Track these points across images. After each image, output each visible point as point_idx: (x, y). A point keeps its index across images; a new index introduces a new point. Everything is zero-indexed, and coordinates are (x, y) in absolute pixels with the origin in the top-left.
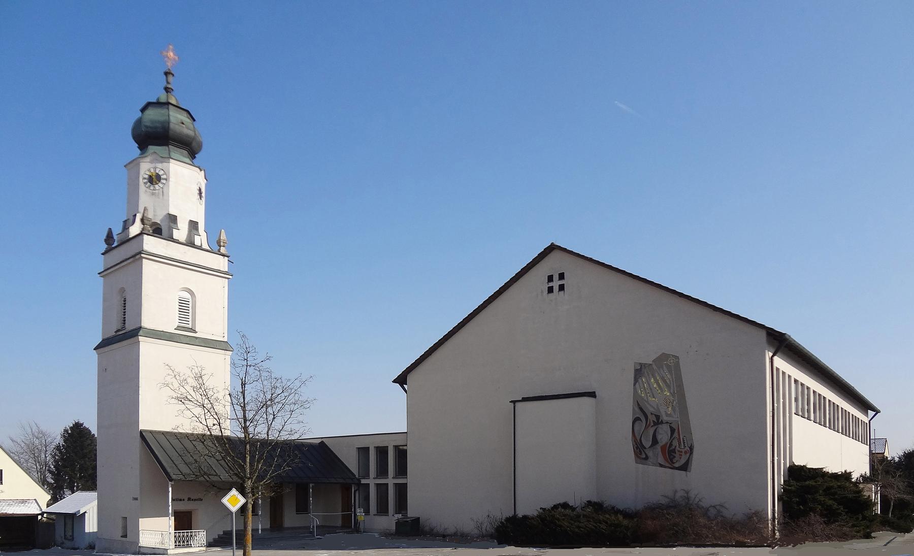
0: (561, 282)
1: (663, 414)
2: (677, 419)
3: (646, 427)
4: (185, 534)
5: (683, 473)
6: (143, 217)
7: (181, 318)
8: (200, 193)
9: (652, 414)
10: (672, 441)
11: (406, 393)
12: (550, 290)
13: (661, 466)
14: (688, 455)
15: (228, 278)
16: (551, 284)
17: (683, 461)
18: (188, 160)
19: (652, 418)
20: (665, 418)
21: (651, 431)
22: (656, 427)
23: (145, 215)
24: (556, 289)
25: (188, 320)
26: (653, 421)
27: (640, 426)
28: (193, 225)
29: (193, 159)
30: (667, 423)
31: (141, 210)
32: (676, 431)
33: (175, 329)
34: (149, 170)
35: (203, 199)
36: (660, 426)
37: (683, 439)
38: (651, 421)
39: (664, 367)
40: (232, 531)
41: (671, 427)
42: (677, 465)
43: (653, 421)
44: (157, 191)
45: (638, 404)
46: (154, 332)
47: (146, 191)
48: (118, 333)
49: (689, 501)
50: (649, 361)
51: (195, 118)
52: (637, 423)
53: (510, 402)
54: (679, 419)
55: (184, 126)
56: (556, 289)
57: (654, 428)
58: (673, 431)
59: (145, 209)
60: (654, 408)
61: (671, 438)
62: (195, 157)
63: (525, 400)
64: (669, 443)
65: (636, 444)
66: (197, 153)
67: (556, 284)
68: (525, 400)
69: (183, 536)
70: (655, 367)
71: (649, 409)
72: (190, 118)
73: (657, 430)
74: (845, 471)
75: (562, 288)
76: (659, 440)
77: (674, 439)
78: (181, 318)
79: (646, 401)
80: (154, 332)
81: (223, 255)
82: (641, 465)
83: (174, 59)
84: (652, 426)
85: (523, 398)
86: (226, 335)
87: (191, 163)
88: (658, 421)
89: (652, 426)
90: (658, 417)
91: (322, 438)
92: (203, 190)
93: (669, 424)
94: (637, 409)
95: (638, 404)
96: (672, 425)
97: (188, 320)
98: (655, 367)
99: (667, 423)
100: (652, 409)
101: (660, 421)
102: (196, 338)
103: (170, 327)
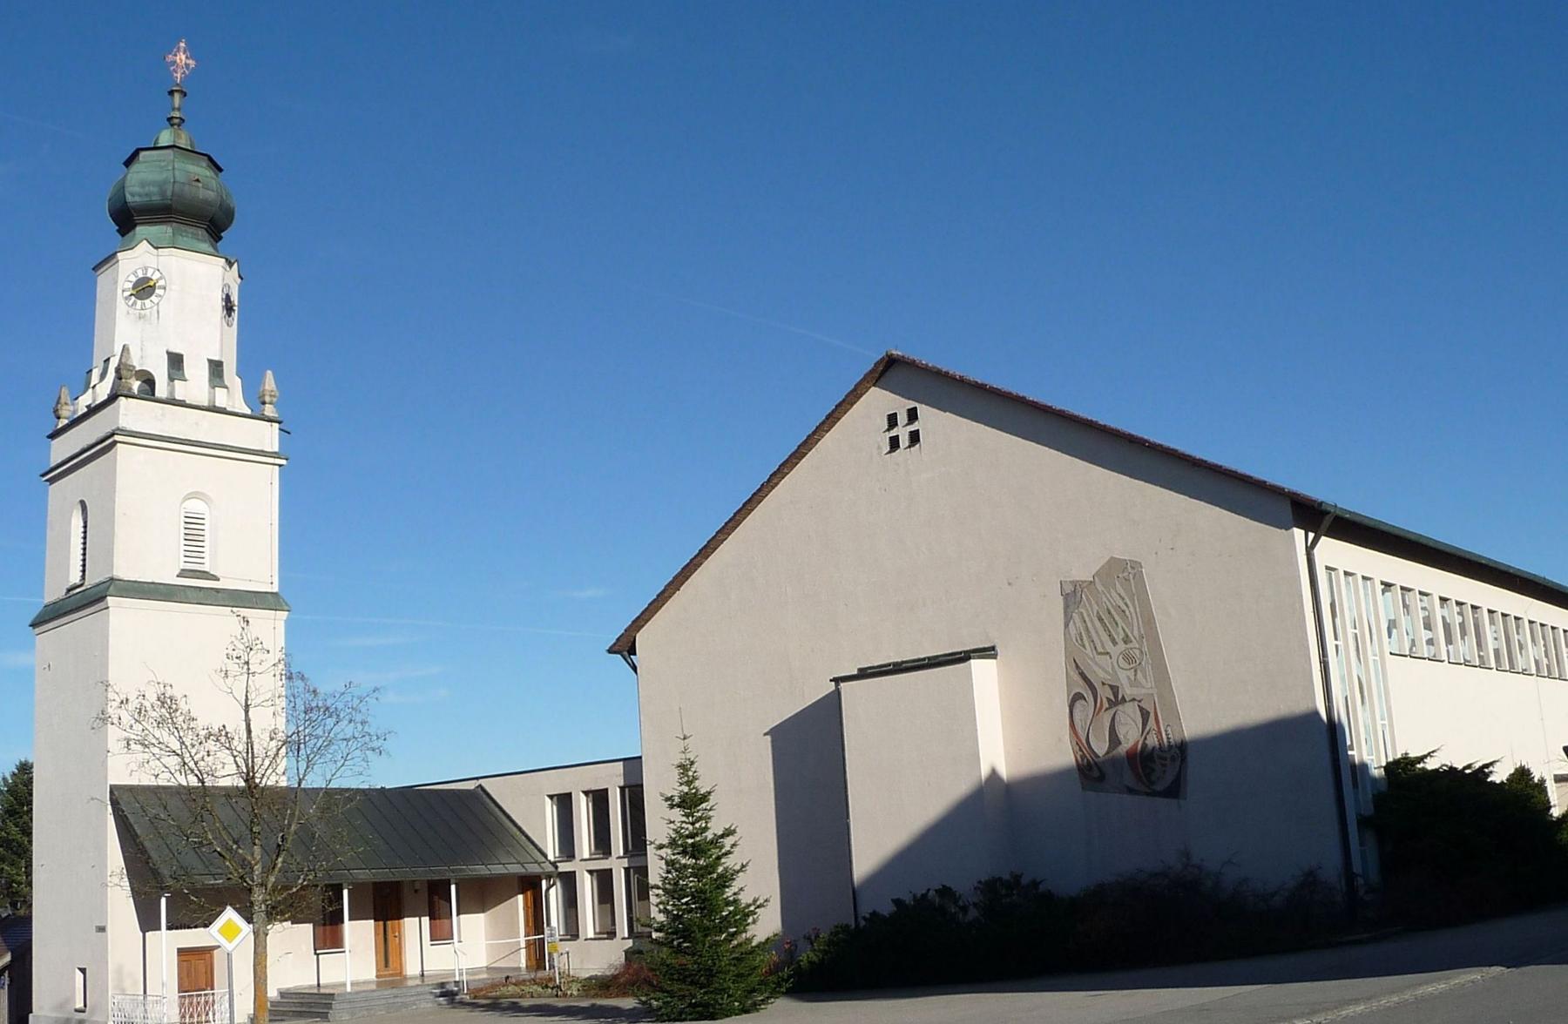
0: (912, 428)
1: (1124, 681)
2: (1150, 691)
3: (1097, 712)
4: (203, 998)
5: (1173, 802)
6: (119, 365)
7: (188, 554)
8: (229, 308)
9: (1103, 684)
10: (1145, 738)
11: (636, 672)
12: (894, 443)
13: (1131, 791)
14: (1178, 763)
15: (280, 466)
16: (893, 433)
17: (1169, 778)
18: (206, 246)
19: (1105, 693)
20: (1127, 691)
21: (1106, 719)
22: (1114, 710)
23: (123, 361)
24: (904, 441)
25: (202, 555)
26: (1107, 698)
27: (1084, 711)
28: (216, 368)
29: (217, 242)
30: (1134, 700)
31: (118, 350)
32: (1152, 715)
33: (178, 576)
34: (135, 273)
35: (235, 315)
36: (1120, 707)
37: (1166, 731)
38: (1105, 700)
39: (1118, 585)
40: (458, 914)
41: (1141, 709)
42: (1159, 788)
43: (1107, 698)
44: (147, 312)
45: (1077, 666)
46: (136, 585)
47: (128, 313)
48: (72, 593)
49: (1188, 859)
50: (1085, 575)
51: (220, 165)
52: (1079, 704)
53: (831, 680)
54: (1154, 691)
55: (200, 185)
56: (904, 441)
57: (1112, 712)
58: (1145, 715)
59: (125, 349)
60: (1107, 672)
61: (1143, 733)
62: (220, 238)
63: (864, 674)
64: (1141, 743)
65: (1081, 750)
66: (223, 231)
67: (903, 432)
68: (864, 674)
69: (198, 1003)
70: (1100, 588)
71: (1098, 675)
72: (213, 167)
73: (1117, 717)
74: (898, 902)
75: (915, 438)
76: (1121, 737)
77: (1148, 733)
78: (188, 554)
79: (1090, 658)
80: (136, 585)
81: (270, 420)
82: (1091, 794)
83: (187, 65)
84: (1107, 709)
85: (860, 670)
86: (276, 580)
87: (211, 250)
88: (1117, 700)
89: (1107, 709)
90: (1115, 689)
91: (477, 778)
92: (235, 298)
93: (1136, 703)
94: (1077, 677)
95: (1077, 666)
96: (1142, 704)
97: (202, 555)
98: (1100, 588)
99: (1134, 700)
100: (1102, 674)
101: (1120, 697)
102: (217, 590)
103: (168, 575)
